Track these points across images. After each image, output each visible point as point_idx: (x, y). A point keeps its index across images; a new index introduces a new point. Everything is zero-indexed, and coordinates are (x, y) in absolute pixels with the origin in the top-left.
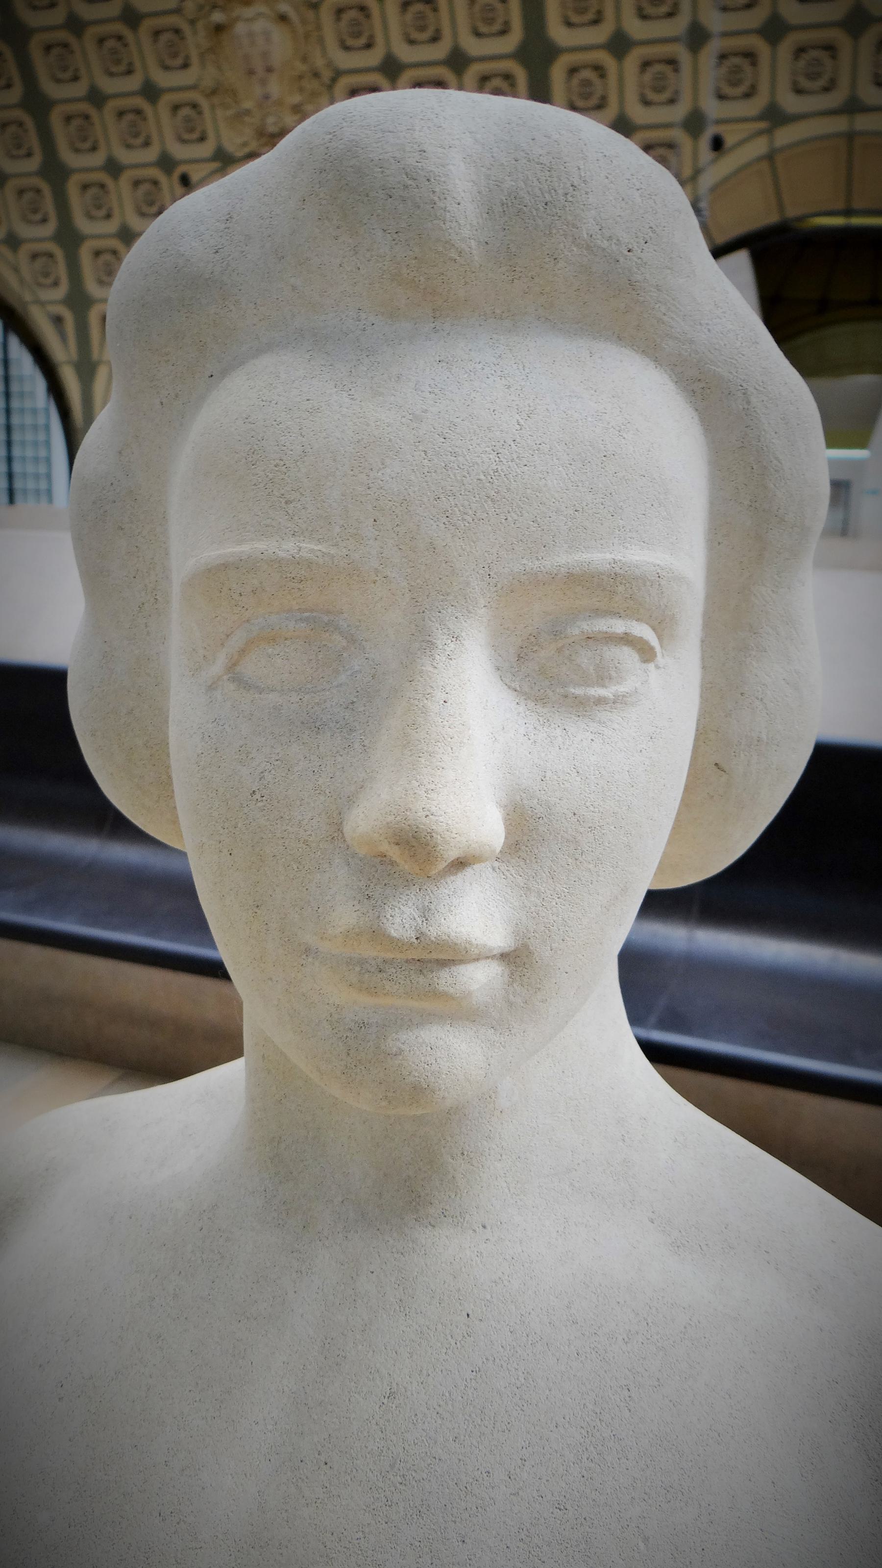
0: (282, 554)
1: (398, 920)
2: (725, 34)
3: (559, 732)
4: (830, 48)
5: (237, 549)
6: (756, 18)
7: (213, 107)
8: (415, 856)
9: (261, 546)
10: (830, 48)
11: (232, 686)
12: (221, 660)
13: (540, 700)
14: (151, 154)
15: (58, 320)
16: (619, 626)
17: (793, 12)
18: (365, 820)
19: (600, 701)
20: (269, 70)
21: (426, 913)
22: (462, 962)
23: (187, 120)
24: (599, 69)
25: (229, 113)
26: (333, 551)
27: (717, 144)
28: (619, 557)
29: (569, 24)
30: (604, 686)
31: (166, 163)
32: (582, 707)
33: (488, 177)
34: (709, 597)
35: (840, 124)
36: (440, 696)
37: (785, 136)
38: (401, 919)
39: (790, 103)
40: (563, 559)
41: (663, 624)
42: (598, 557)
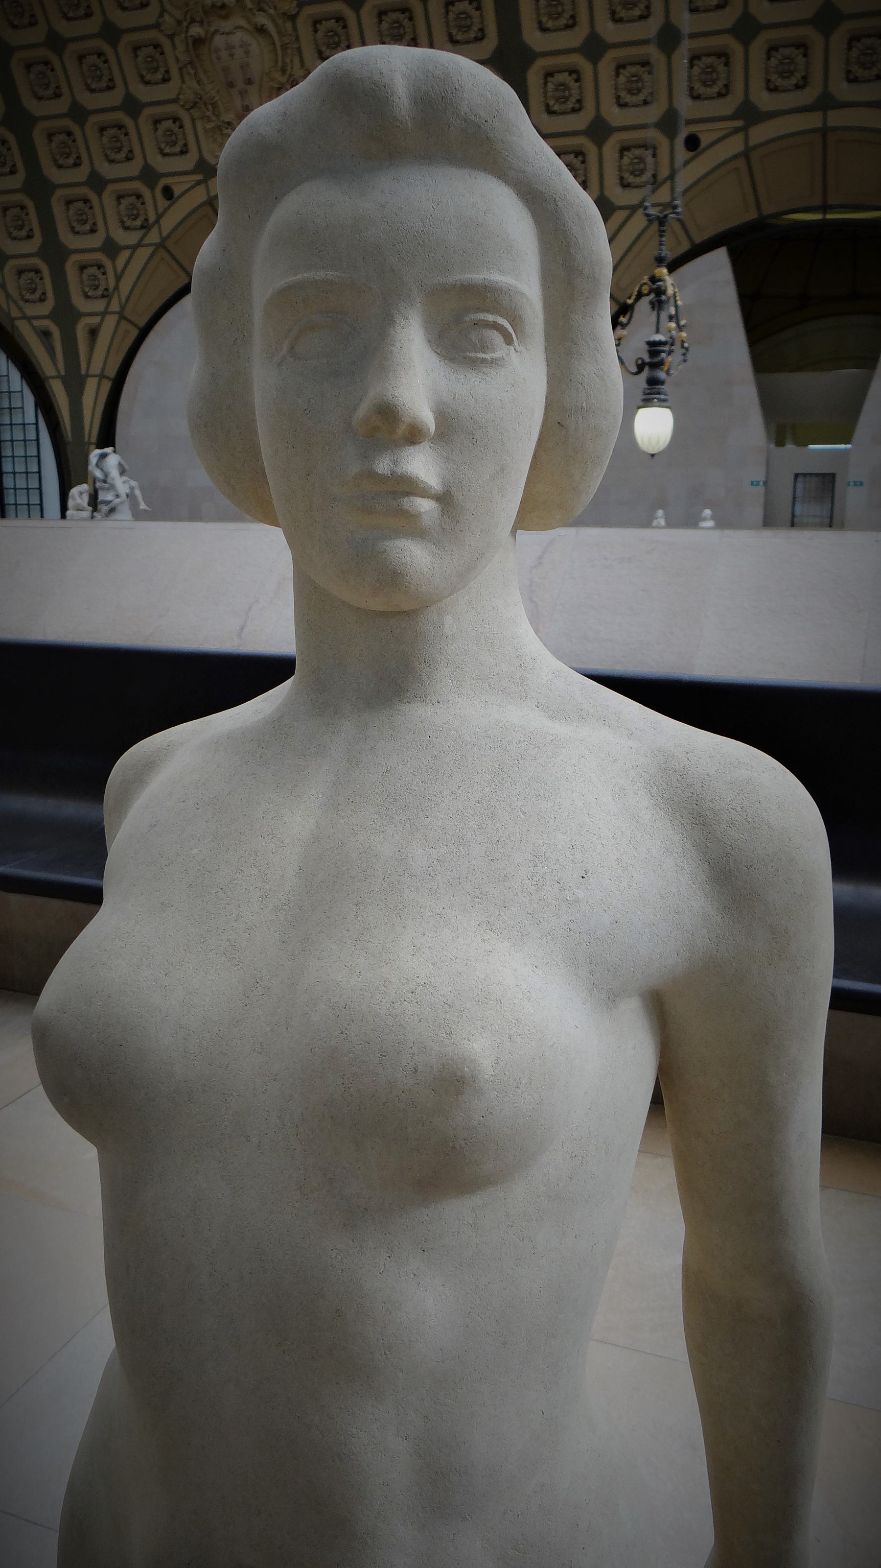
0: (317, 278)
1: (381, 465)
2: (692, 36)
3: (462, 376)
4: (802, 46)
5: (295, 278)
6: (728, 17)
7: (193, 120)
8: (390, 428)
9: (306, 275)
10: (802, 46)
11: (292, 360)
12: (285, 348)
13: (452, 360)
14: (134, 168)
15: (45, 334)
16: (490, 318)
17: (763, 11)
18: (362, 411)
19: (484, 361)
20: (249, 82)
21: (395, 463)
22: (415, 495)
23: (170, 132)
24: (575, 72)
25: (210, 126)
26: (343, 275)
27: (692, 143)
28: (487, 277)
29: (543, 29)
30: (485, 353)
31: (149, 176)
32: (475, 364)
33: (414, 85)
34: (546, 321)
35: (814, 120)
36: (398, 345)
37: (759, 133)
38: (383, 465)
39: (764, 100)
40: (458, 277)
41: (516, 320)
42: (477, 277)
